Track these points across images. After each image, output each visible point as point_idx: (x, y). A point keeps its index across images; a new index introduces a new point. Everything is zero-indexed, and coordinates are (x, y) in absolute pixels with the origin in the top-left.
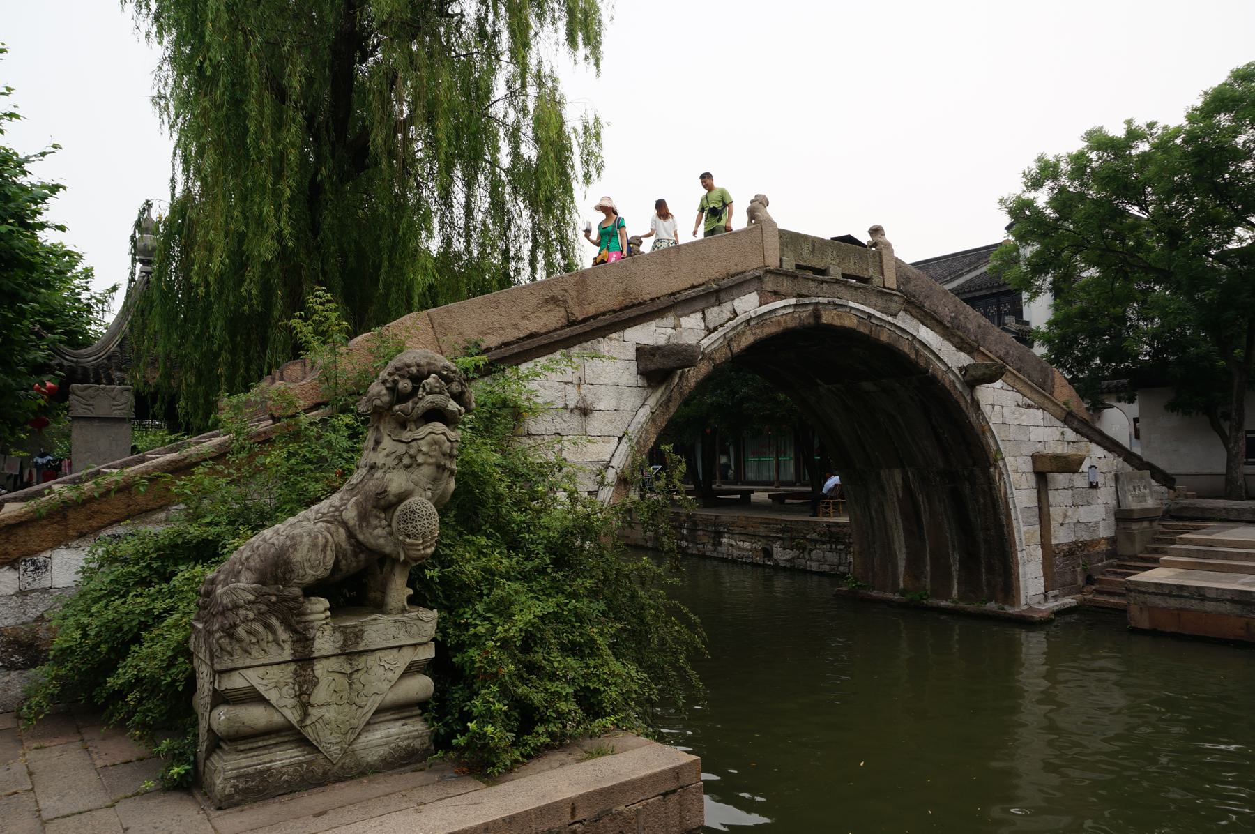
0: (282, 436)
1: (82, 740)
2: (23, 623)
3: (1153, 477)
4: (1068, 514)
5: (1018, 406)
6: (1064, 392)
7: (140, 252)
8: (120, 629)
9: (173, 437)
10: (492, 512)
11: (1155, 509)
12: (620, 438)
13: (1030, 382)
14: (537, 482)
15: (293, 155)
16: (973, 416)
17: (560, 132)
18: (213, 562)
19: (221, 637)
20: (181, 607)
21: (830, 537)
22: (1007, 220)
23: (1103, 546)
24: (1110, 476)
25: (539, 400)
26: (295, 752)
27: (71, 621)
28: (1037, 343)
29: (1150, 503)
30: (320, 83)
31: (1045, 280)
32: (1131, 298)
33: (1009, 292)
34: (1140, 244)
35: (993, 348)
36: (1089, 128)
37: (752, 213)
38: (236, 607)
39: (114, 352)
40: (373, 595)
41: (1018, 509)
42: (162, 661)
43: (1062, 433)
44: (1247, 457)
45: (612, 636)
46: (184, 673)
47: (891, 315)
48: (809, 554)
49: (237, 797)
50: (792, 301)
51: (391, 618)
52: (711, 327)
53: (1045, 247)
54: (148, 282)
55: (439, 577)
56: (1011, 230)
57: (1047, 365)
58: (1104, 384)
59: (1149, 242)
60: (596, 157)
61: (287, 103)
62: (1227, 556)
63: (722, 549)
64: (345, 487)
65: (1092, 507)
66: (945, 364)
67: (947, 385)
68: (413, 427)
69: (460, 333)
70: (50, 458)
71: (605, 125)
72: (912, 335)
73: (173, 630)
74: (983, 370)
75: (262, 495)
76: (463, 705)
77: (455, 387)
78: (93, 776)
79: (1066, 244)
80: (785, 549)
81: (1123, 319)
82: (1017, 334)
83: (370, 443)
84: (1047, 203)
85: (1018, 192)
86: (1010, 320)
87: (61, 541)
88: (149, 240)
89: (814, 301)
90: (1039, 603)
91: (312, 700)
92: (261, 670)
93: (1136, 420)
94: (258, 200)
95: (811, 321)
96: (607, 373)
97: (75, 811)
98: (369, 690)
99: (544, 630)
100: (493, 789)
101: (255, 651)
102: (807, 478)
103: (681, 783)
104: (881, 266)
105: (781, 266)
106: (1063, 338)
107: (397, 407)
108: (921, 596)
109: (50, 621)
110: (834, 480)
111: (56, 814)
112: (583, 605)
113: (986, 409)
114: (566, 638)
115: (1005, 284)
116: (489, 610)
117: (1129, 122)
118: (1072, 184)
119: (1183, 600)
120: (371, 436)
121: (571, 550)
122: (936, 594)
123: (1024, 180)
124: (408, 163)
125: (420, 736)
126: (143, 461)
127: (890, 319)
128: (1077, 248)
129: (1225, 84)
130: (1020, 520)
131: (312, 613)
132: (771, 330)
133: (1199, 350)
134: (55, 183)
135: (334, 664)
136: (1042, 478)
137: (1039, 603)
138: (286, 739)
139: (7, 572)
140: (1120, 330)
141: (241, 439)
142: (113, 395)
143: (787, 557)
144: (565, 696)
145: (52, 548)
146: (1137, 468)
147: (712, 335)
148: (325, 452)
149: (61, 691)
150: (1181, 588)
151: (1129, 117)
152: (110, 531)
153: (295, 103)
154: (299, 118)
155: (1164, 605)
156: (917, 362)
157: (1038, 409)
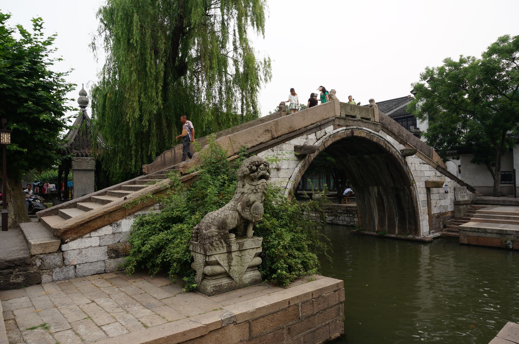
2: (114, 244)
3: (467, 189)
4: (438, 203)
5: (420, 163)
6: (436, 158)
11: (468, 201)
13: (425, 155)
16: (405, 167)
18: (184, 223)
21: (347, 212)
23: (450, 214)
24: (452, 188)
29: (466, 198)
32: (459, 120)
43: (436, 173)
44: (501, 181)
48: (339, 218)
49: (214, 293)
50: (345, 128)
58: (448, 152)
62: (494, 217)
65: (446, 200)
66: (395, 149)
69: (239, 143)
70: (39, 183)
74: (409, 151)
80: (329, 216)
82: (415, 133)
86: (412, 128)
87: (124, 217)
89: (352, 128)
90: (427, 235)
92: (219, 255)
93: (459, 166)
94: (150, 91)
95: (351, 135)
98: (246, 261)
100: (285, 290)
103: (339, 288)
104: (374, 114)
105: (341, 116)
106: (433, 136)
107: (252, 175)
108: (384, 233)
110: (348, 190)
113: (409, 165)
114: (296, 246)
117: (461, 56)
119: (479, 233)
123: (420, 76)
125: (259, 276)
127: (377, 133)
129: (496, 43)
130: (421, 205)
132: (338, 138)
135: (237, 253)
136: (428, 190)
137: (427, 235)
138: (224, 276)
139: (109, 227)
142: (88, 161)
143: (330, 219)
145: (121, 219)
146: (462, 186)
147: (319, 141)
150: (478, 229)
155: (472, 235)
157: (427, 164)
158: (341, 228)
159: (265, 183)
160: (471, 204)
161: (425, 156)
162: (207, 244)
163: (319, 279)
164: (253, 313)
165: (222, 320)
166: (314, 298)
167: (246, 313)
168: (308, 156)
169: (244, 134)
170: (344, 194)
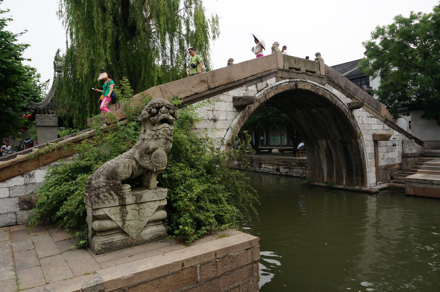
0: (111, 130)
1: (49, 233)
2: (27, 195)
5: (368, 117)
6: (384, 111)
7: (57, 68)
8: (60, 196)
9: (74, 130)
10: (185, 155)
11: (416, 153)
12: (227, 130)
14: (200, 145)
15: (110, 31)
16: (352, 121)
17: (204, 21)
18: (90, 173)
19: (95, 198)
20: (80, 189)
22: (365, 50)
23: (397, 166)
24: (400, 142)
25: (199, 117)
26: (121, 236)
27: (43, 193)
28: (374, 95)
29: (414, 151)
30: (118, 5)
31: (378, 72)
32: (409, 78)
33: (365, 77)
34: (413, 58)
35: (359, 96)
36: (396, 15)
37: (273, 49)
38: (99, 187)
39: (49, 103)
40: (144, 184)
41: (367, 153)
42: (75, 206)
43: (384, 127)
45: (227, 197)
46: (82, 210)
47: (323, 85)
49: (102, 251)
50: (288, 80)
51: (152, 191)
52: (259, 90)
53: (379, 60)
54: (60, 78)
55: (167, 177)
56: (366, 54)
57: (379, 102)
58: (399, 109)
59: (417, 58)
60: (217, 30)
61: (107, 12)
63: (262, 169)
64: (134, 147)
65: (394, 152)
66: (342, 102)
67: (343, 110)
68: (157, 125)
69: (171, 93)
71: (220, 18)
72: (330, 92)
73: (78, 196)
74: (356, 104)
75: (105, 150)
76: (177, 220)
77: (171, 111)
78: (54, 244)
79: (386, 58)
81: (406, 86)
83: (142, 131)
84: (380, 43)
85: (369, 40)
86: (365, 87)
87: (38, 167)
88: (60, 64)
91: (126, 219)
92: (109, 209)
93: (410, 122)
95: (294, 87)
96: (223, 107)
97: (49, 255)
98: (145, 215)
99: (204, 195)
100: (188, 248)
101: (106, 202)
102: (292, 144)
103: (252, 246)
104: (320, 67)
105: (284, 68)
106: (384, 93)
107: (151, 118)
109: (36, 194)
110: (302, 144)
111: (43, 257)
112: (217, 186)
113: (357, 118)
114: (211, 198)
115: (363, 74)
116: (185, 188)
117: (412, 12)
118: (389, 36)
119: (425, 185)
120: (143, 129)
121: (212, 168)
122: (337, 184)
123: (371, 35)
124: (149, 34)
125: (163, 231)
126: (63, 140)
127: (322, 86)
128: (390, 60)
130: (368, 157)
131: (125, 190)
132: (280, 91)
133: (434, 96)
134: (27, 44)
135: (133, 207)
136: (376, 143)
139: (20, 178)
140: (405, 90)
141: (98, 131)
142: (50, 118)
143: (285, 171)
144: (212, 217)
145: (35, 169)
146: (410, 139)
148: (126, 135)
149: (41, 217)
150: (425, 180)
151: (412, 11)
152: (54, 163)
153: (109, 12)
154: (111, 18)
155: (419, 186)
156: (332, 102)
157: (375, 118)
158: (295, 179)
159: (168, 127)
160: (419, 156)
161: (373, 110)
162: (93, 196)
163: (232, 235)
164: (129, 279)
165: (82, 289)
166: (218, 258)
167: (120, 279)
168: (248, 108)
169: (177, 84)
170: (298, 148)
